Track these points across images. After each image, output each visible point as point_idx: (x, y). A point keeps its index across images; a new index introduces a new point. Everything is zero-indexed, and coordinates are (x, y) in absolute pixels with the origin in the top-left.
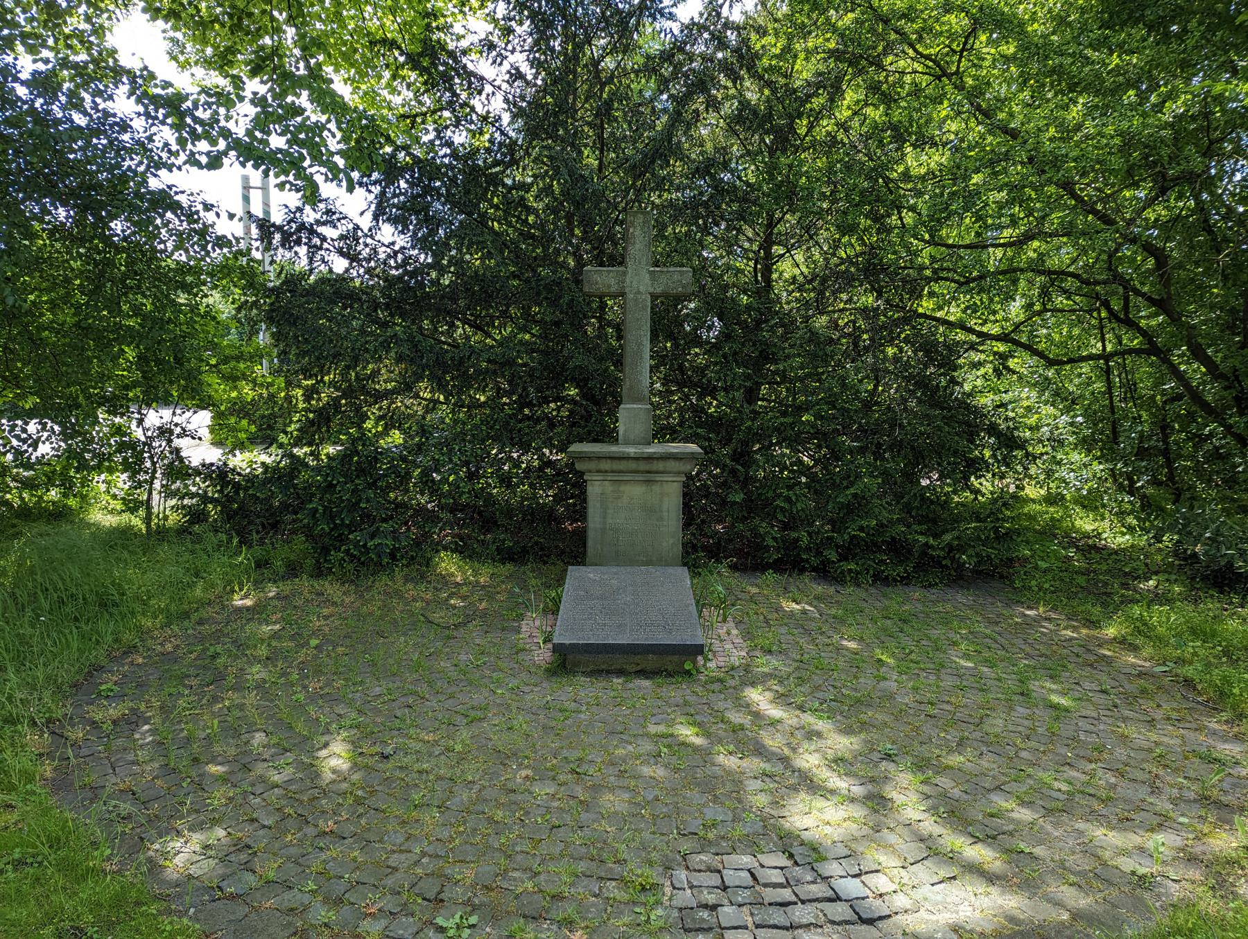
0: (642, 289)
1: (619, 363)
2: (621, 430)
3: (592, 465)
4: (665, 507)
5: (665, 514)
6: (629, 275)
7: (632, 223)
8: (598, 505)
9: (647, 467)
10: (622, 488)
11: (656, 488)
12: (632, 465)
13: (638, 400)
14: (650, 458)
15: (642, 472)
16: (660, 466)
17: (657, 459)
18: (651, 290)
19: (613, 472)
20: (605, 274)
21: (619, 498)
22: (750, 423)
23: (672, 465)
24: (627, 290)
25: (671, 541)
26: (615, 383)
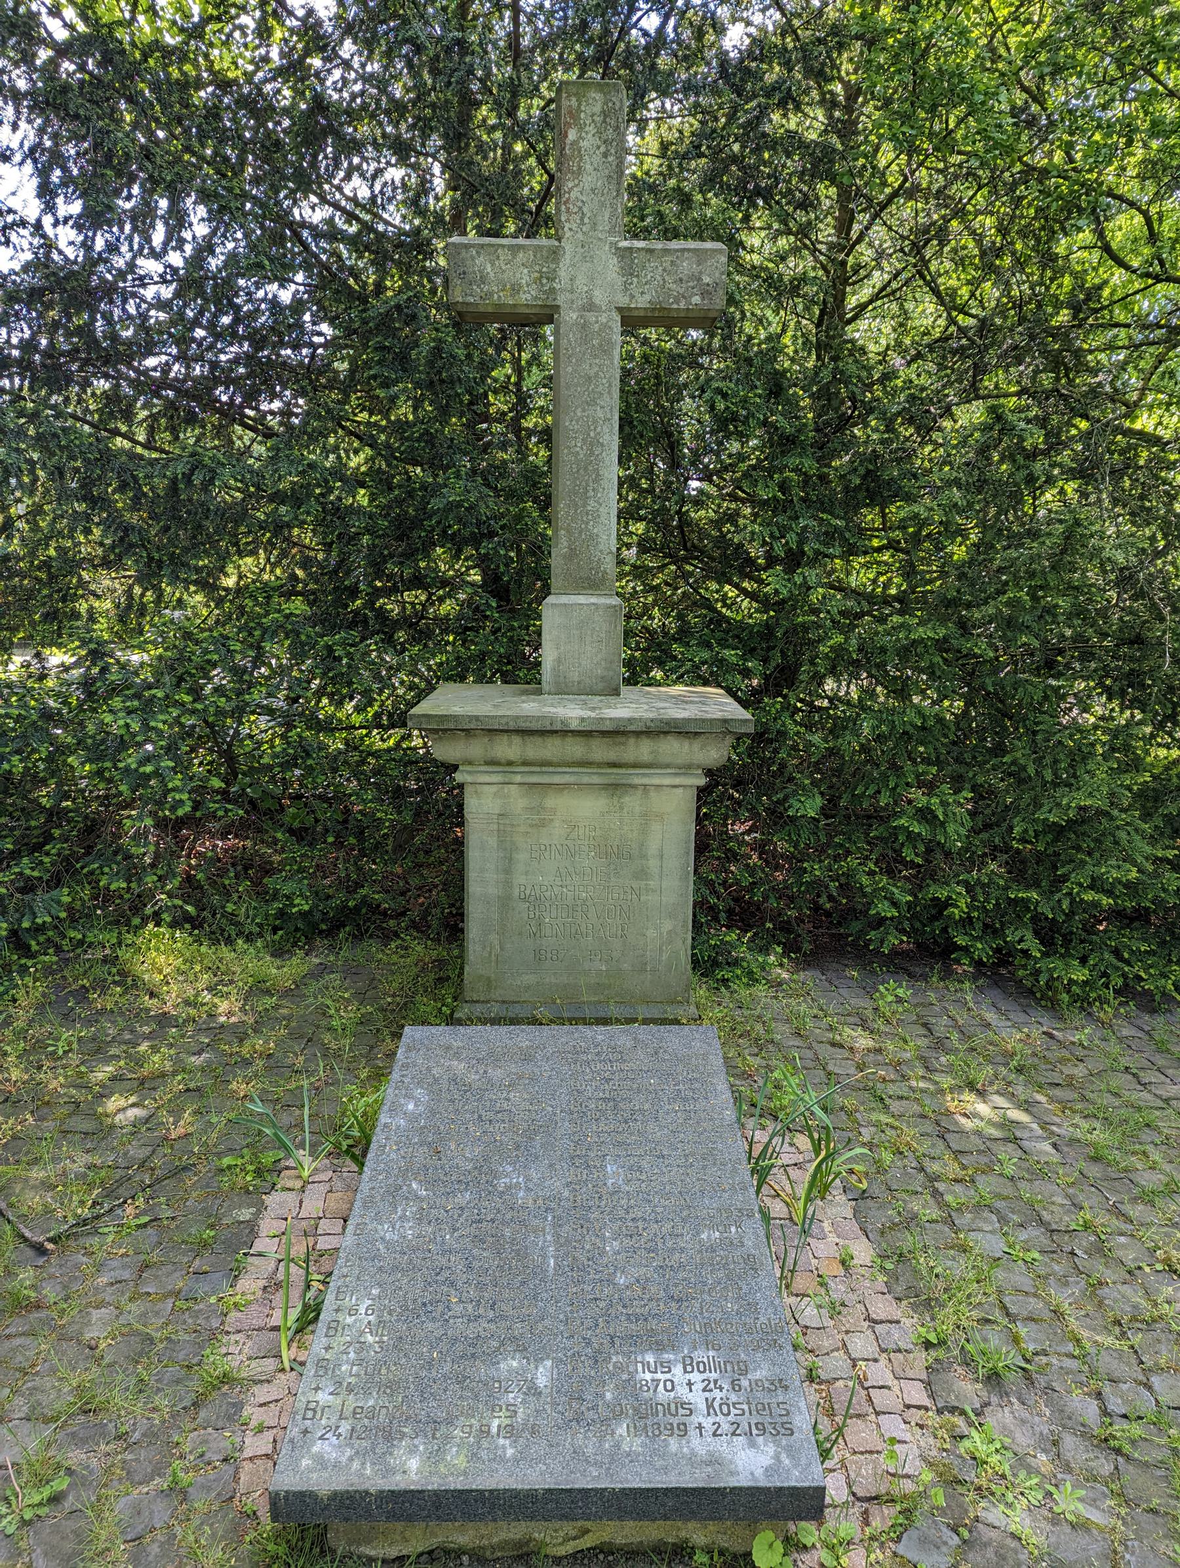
0: (599, 297)
1: (545, 504)
2: (549, 655)
3: (476, 749)
4: (653, 847)
5: (653, 863)
6: (566, 260)
7: (574, 115)
8: (493, 842)
9: (612, 755)
10: (551, 801)
11: (632, 802)
12: (575, 749)
13: (592, 584)
14: (618, 733)
15: (600, 765)
16: (643, 750)
17: (638, 734)
18: (623, 301)
19: (525, 763)
20: (504, 255)
21: (543, 824)
22: (840, 639)
23: (673, 748)
24: (561, 300)
25: (668, 925)
26: (540, 549)
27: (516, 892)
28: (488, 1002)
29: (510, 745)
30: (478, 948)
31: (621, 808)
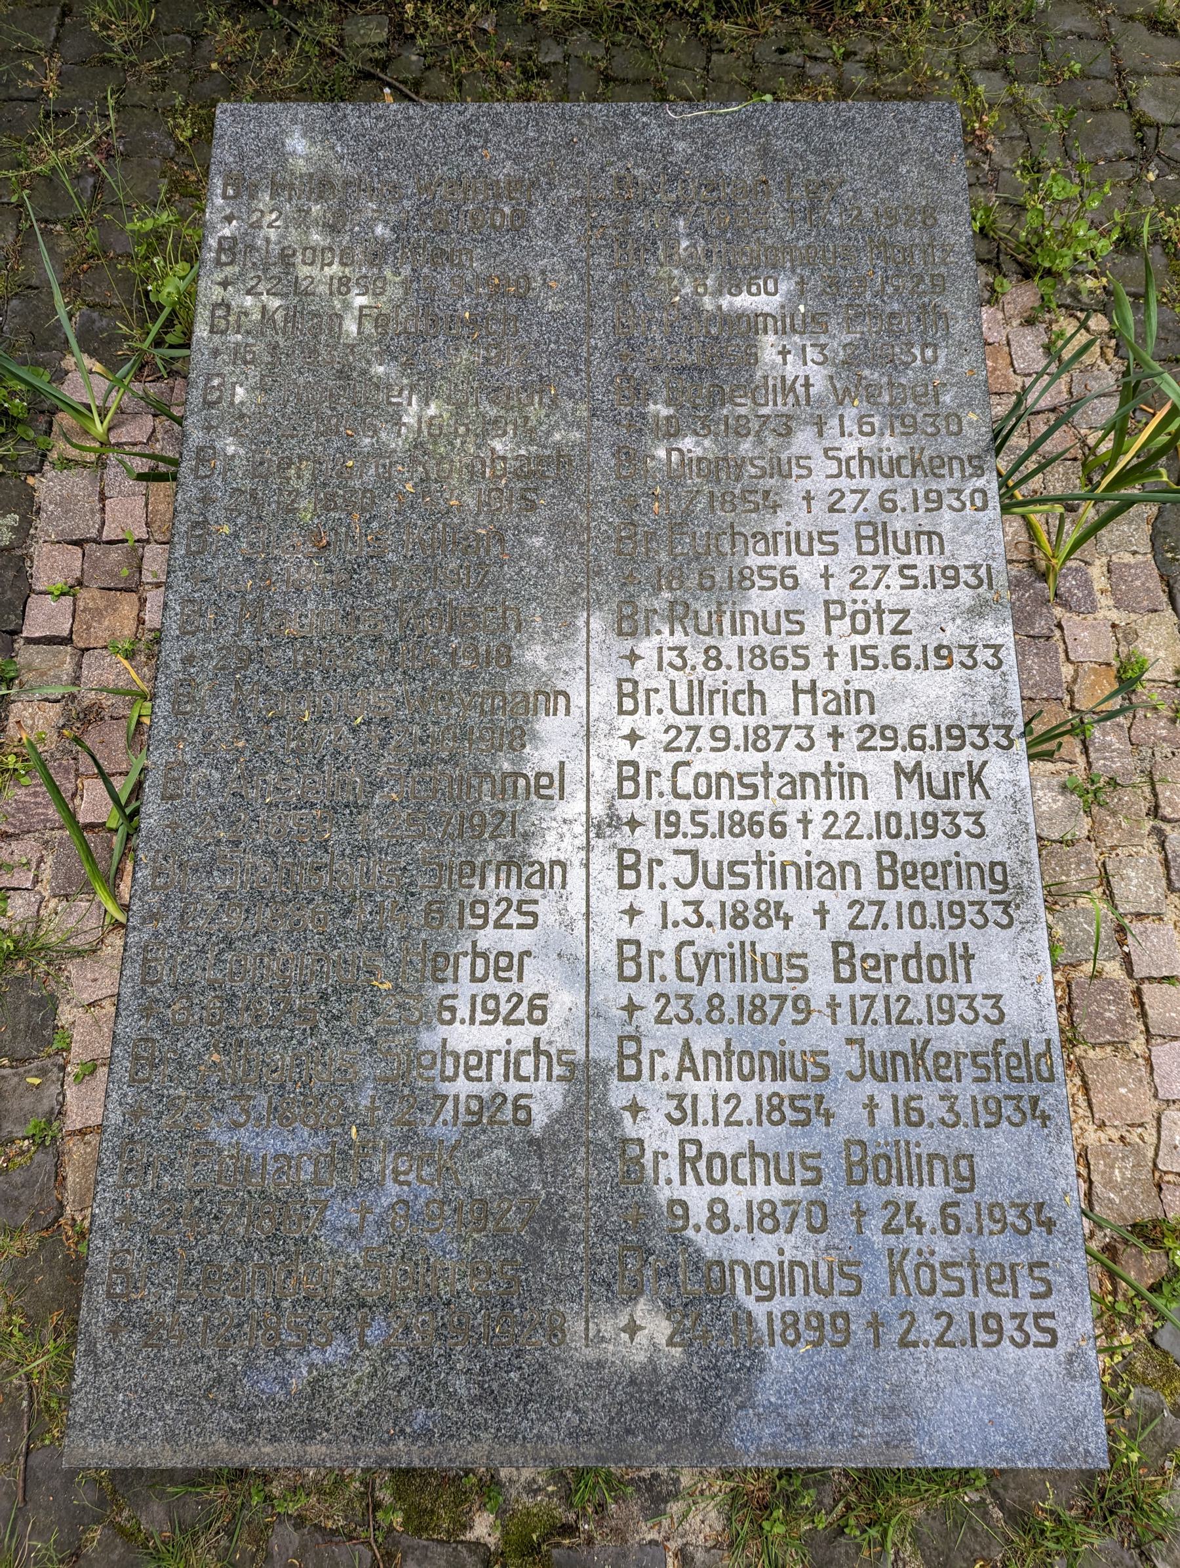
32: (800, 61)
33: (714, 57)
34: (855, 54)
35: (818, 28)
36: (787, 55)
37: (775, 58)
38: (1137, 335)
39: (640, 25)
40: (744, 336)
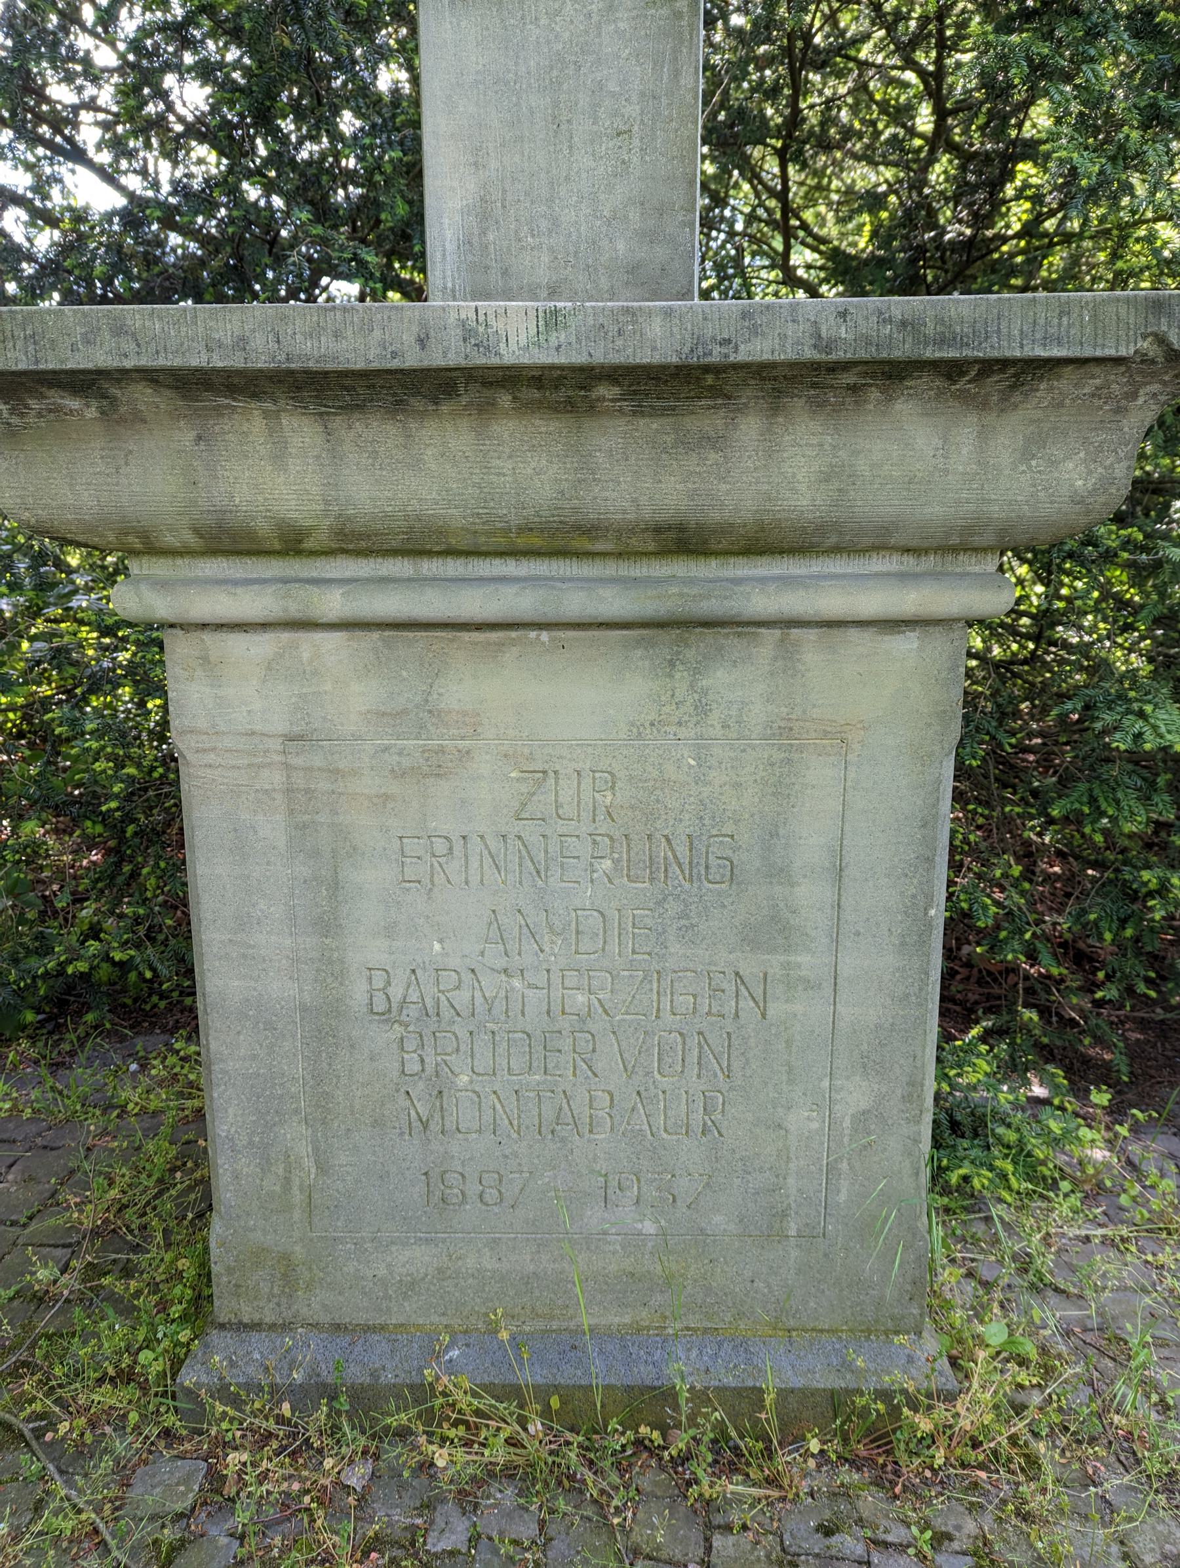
27: (358, 992)
28: (286, 1327)
29: (279, 458)
30: (246, 1165)
31: (702, 710)
32: (860, 1550)
33: (718, 1541)
34: (949, 1537)
35: (877, 1483)
36: (836, 1539)
37: (817, 1543)
38: (42, 1419)
39: (592, 1485)
40: (226, 181)
